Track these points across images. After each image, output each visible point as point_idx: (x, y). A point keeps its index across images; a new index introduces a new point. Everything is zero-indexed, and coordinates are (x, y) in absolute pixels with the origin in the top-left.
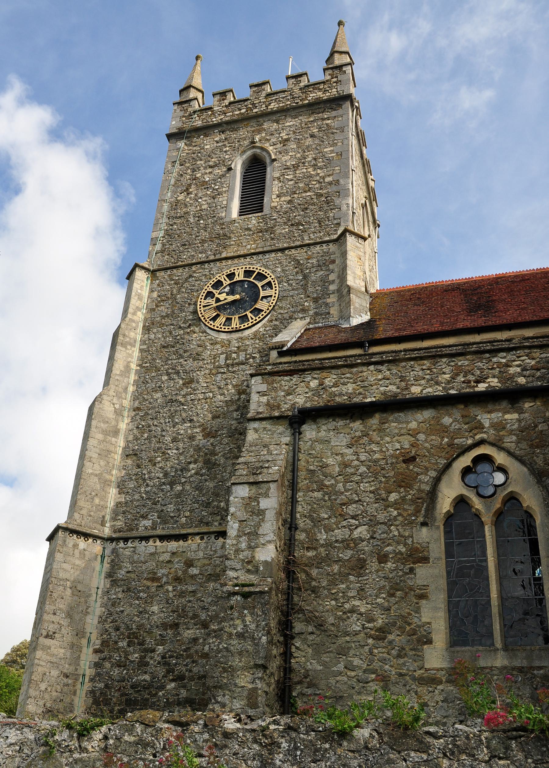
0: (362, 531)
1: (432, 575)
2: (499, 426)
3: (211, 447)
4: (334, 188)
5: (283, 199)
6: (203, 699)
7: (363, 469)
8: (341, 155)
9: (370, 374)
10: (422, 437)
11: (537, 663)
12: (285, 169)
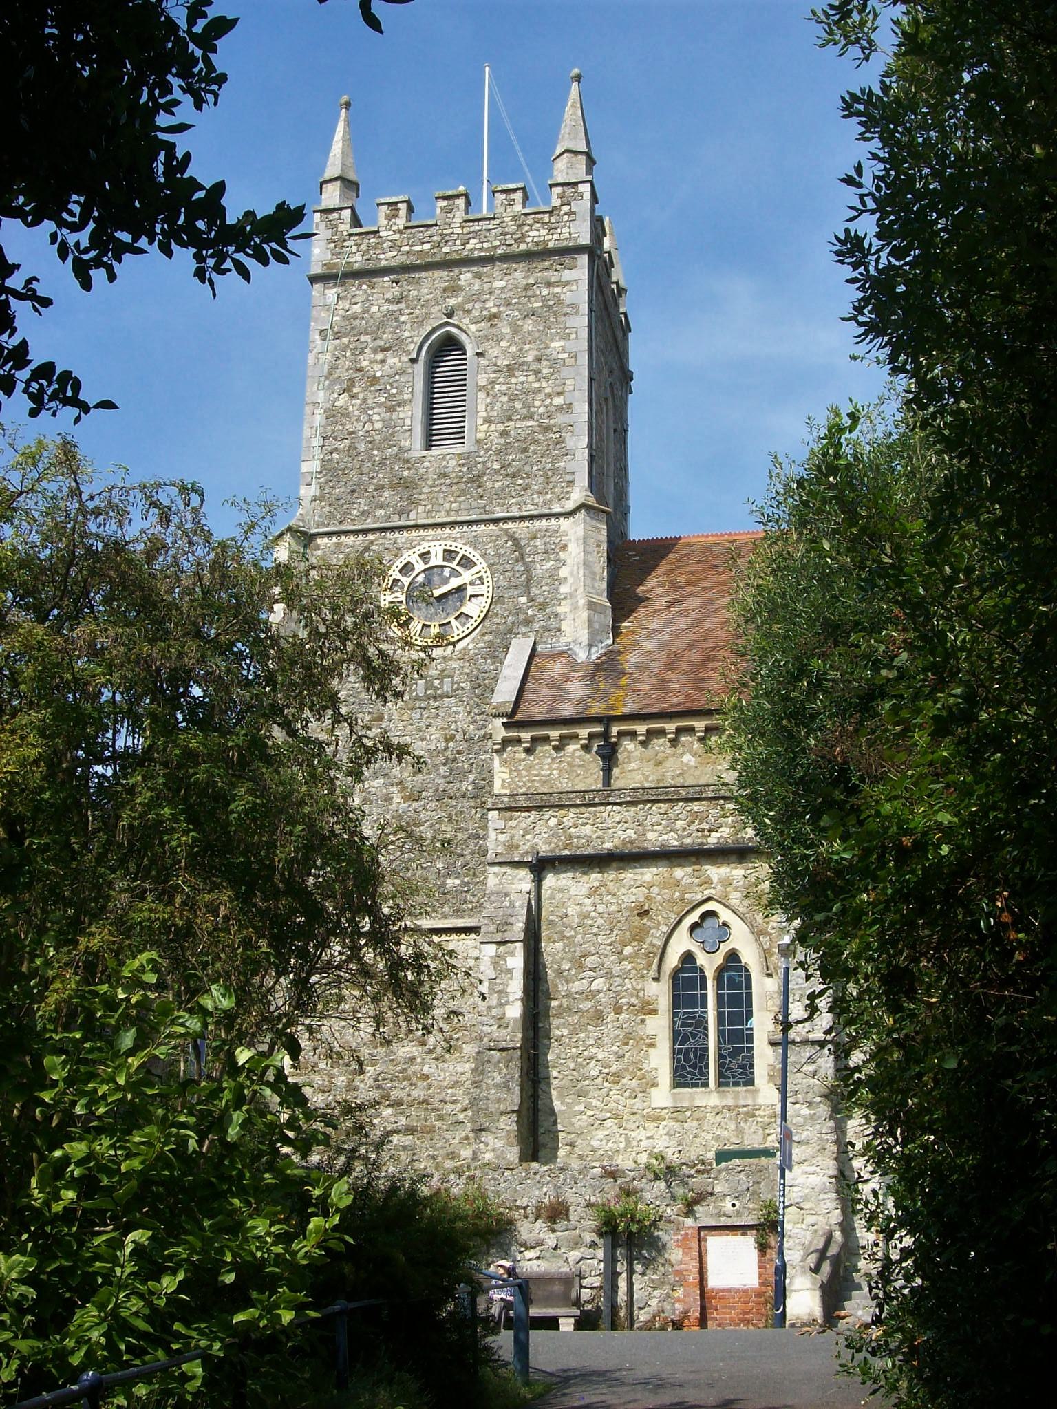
0: (599, 984)
1: (659, 1026)
2: (726, 882)
3: (414, 815)
4: (561, 419)
5: (493, 427)
6: (426, 1127)
7: (600, 921)
8: (576, 357)
9: (612, 815)
10: (655, 890)
11: (742, 1103)
12: (495, 372)
